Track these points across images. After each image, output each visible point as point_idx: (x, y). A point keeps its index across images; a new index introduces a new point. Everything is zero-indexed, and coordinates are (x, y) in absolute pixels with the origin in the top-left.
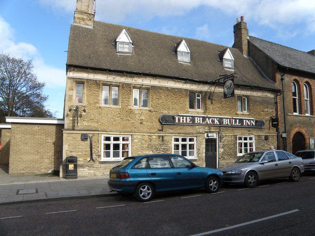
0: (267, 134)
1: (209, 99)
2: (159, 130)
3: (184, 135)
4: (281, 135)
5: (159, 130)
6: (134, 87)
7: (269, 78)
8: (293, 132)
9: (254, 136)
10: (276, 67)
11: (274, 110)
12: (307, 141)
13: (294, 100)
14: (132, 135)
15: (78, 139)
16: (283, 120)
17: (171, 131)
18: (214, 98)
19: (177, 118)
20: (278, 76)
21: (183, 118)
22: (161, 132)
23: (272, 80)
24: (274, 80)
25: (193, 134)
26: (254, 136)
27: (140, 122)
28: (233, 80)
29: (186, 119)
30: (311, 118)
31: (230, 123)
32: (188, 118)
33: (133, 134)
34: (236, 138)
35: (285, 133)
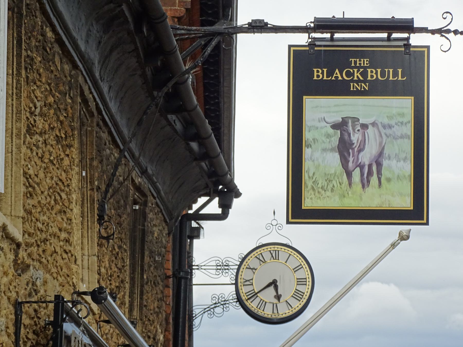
19: (352, 84)
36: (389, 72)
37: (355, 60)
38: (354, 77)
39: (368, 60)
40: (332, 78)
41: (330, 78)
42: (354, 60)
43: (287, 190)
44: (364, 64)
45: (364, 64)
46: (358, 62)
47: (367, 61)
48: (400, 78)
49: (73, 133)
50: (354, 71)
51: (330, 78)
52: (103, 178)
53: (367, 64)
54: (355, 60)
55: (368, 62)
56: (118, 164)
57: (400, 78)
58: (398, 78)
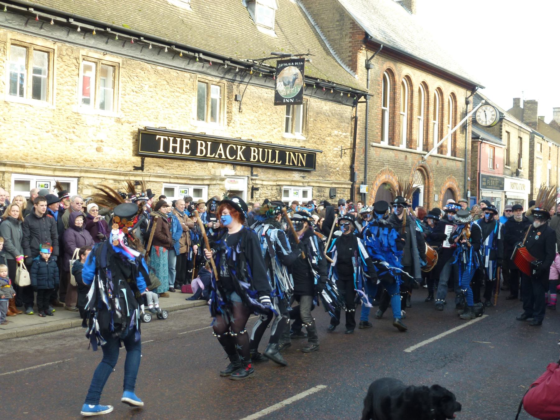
0: (334, 186)
1: (236, 100)
2: (136, 168)
3: (168, 180)
4: (359, 189)
5: (136, 168)
6: (493, 186)
7: (343, 60)
8: (378, 183)
9: (311, 188)
10: (361, 37)
11: (349, 134)
12: (278, 308)
13: (383, 112)
14: (79, 178)
15: (358, 172)
16: (362, 157)
17: (160, 171)
18: (244, 99)
19: (288, 153)
20: (363, 56)
21: (175, 142)
22: (139, 172)
23: (349, 66)
24: (353, 66)
25: (203, 180)
26: (311, 188)
27: (96, 145)
28: (302, 68)
29: (182, 142)
30: (409, 155)
31: (263, 159)
32: (185, 140)
33: (83, 174)
34: (280, 190)
35: (365, 184)
36: (268, 152)
37: (166, 138)
38: (237, 157)
39: (189, 140)
40: (215, 155)
41: (213, 156)
42: (165, 140)
43: (530, 160)
44: (181, 150)
45: (181, 150)
46: (171, 145)
47: (187, 143)
48: (277, 162)
49: (474, 176)
50: (237, 148)
51: (213, 156)
52: (401, 266)
53: (187, 151)
54: (166, 138)
55: (188, 146)
56: (485, 206)
57: (277, 162)
58: (275, 161)
